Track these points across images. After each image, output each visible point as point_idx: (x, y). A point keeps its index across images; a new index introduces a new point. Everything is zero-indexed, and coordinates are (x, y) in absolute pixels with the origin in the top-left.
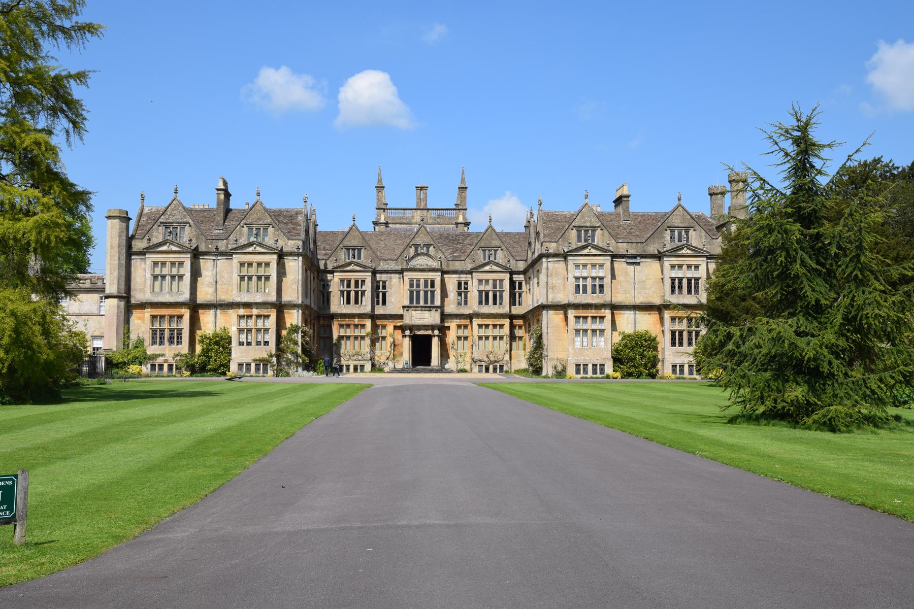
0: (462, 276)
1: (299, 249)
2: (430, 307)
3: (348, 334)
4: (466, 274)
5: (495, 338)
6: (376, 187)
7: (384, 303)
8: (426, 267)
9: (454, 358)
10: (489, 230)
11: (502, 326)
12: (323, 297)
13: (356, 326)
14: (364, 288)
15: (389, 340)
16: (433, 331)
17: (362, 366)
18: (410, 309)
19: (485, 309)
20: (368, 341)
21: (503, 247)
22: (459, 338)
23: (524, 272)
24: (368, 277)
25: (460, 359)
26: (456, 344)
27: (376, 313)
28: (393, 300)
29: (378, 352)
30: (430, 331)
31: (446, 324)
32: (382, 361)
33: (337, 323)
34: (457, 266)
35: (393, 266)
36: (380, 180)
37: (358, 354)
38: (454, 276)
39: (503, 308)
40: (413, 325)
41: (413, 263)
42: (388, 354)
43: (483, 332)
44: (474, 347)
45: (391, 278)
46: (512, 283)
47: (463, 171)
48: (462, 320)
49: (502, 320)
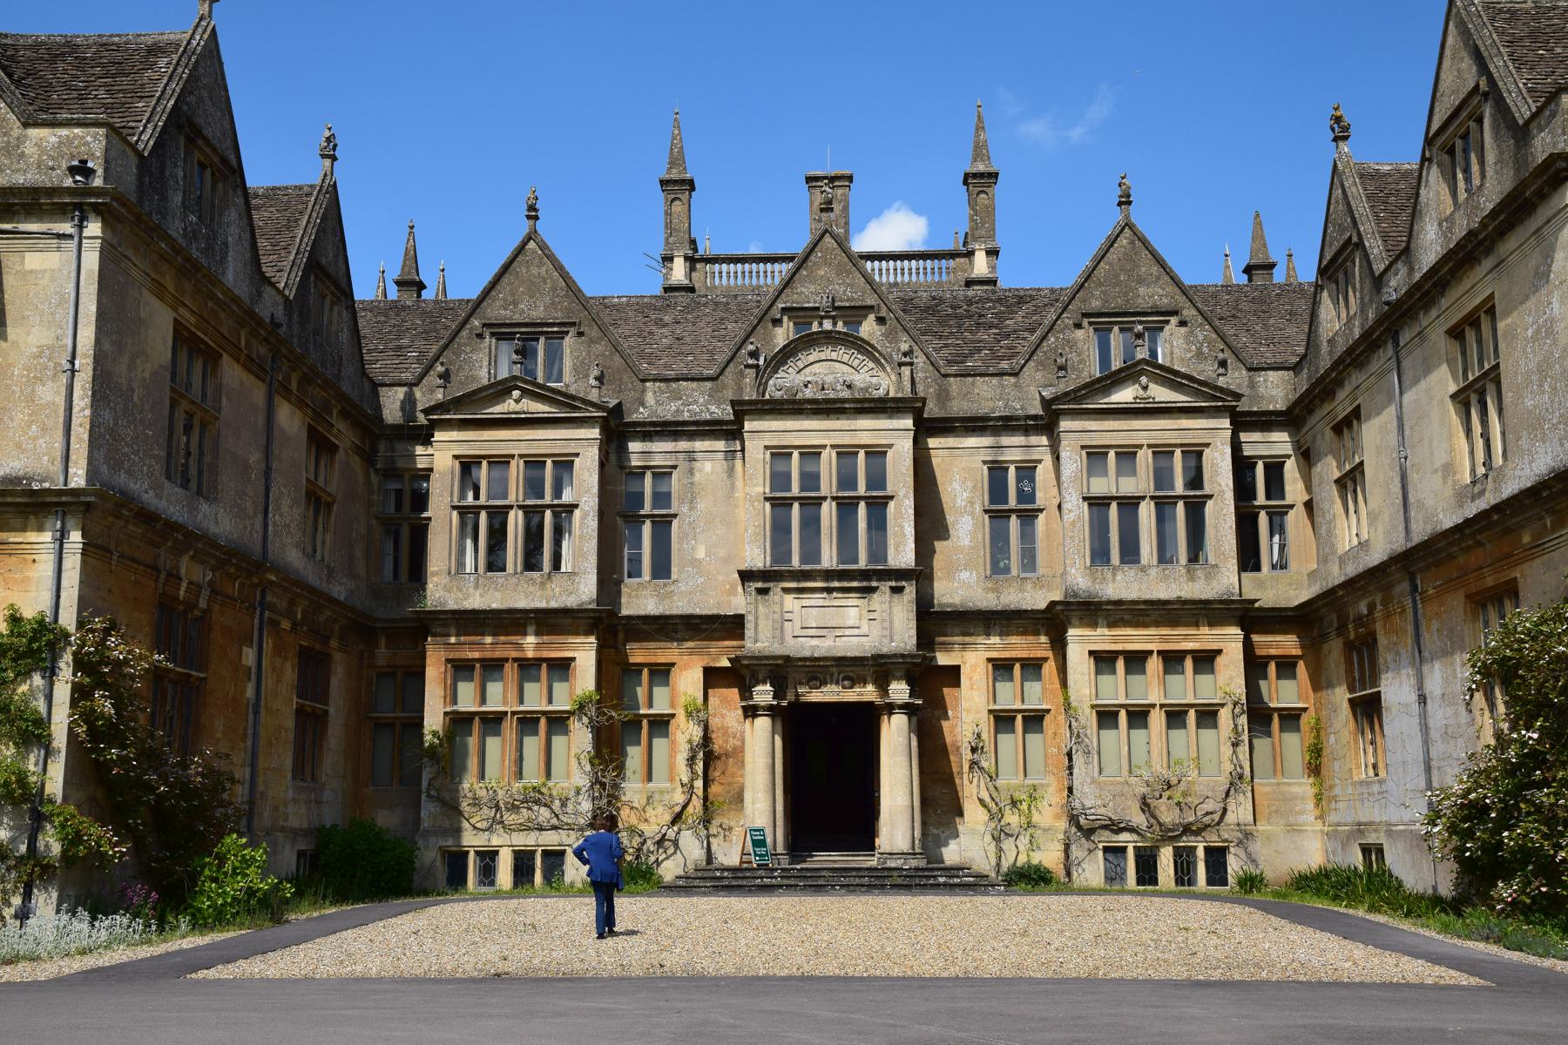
0: (1006, 440)
1: (88, 173)
2: (865, 575)
3: (493, 705)
4: (1027, 430)
5: (1175, 716)
6: (663, 183)
7: (662, 569)
8: (846, 394)
9: (982, 815)
10: (1123, 241)
11: (1206, 660)
12: (396, 549)
13: (528, 668)
14: (567, 497)
15: (686, 732)
16: (883, 689)
17: (554, 858)
18: (777, 588)
19: (1122, 585)
20: (581, 737)
21: (1189, 313)
22: (1003, 720)
23: (1291, 418)
24: (585, 445)
25: (1012, 819)
26: (989, 747)
27: (625, 612)
28: (701, 554)
29: (633, 790)
30: (870, 688)
31: (943, 659)
32: (651, 830)
33: (443, 655)
34: (986, 396)
35: (701, 404)
36: (676, 160)
37: (536, 798)
38: (972, 441)
39: (1209, 577)
40: (787, 659)
41: (786, 380)
42: (679, 798)
43: (1117, 689)
44: (1078, 760)
45: (691, 456)
46: (1242, 466)
47: (980, 118)
48: (1014, 639)
49: (1205, 630)
